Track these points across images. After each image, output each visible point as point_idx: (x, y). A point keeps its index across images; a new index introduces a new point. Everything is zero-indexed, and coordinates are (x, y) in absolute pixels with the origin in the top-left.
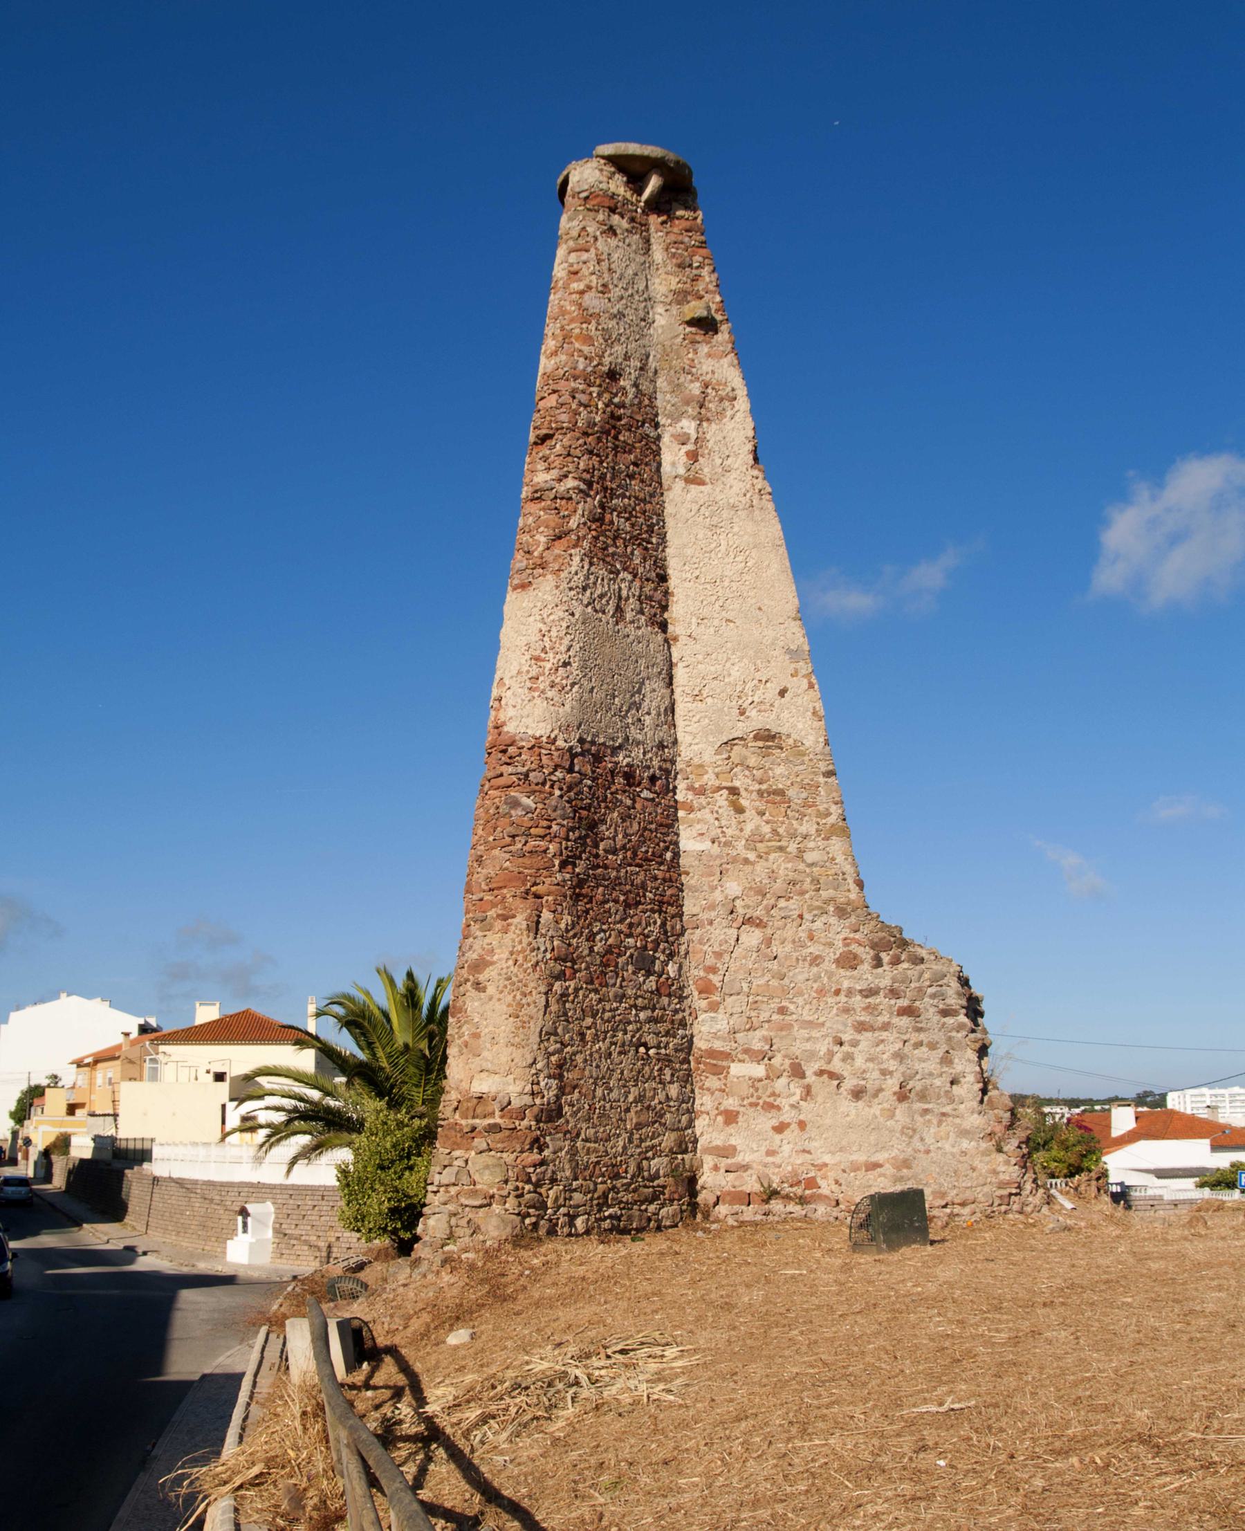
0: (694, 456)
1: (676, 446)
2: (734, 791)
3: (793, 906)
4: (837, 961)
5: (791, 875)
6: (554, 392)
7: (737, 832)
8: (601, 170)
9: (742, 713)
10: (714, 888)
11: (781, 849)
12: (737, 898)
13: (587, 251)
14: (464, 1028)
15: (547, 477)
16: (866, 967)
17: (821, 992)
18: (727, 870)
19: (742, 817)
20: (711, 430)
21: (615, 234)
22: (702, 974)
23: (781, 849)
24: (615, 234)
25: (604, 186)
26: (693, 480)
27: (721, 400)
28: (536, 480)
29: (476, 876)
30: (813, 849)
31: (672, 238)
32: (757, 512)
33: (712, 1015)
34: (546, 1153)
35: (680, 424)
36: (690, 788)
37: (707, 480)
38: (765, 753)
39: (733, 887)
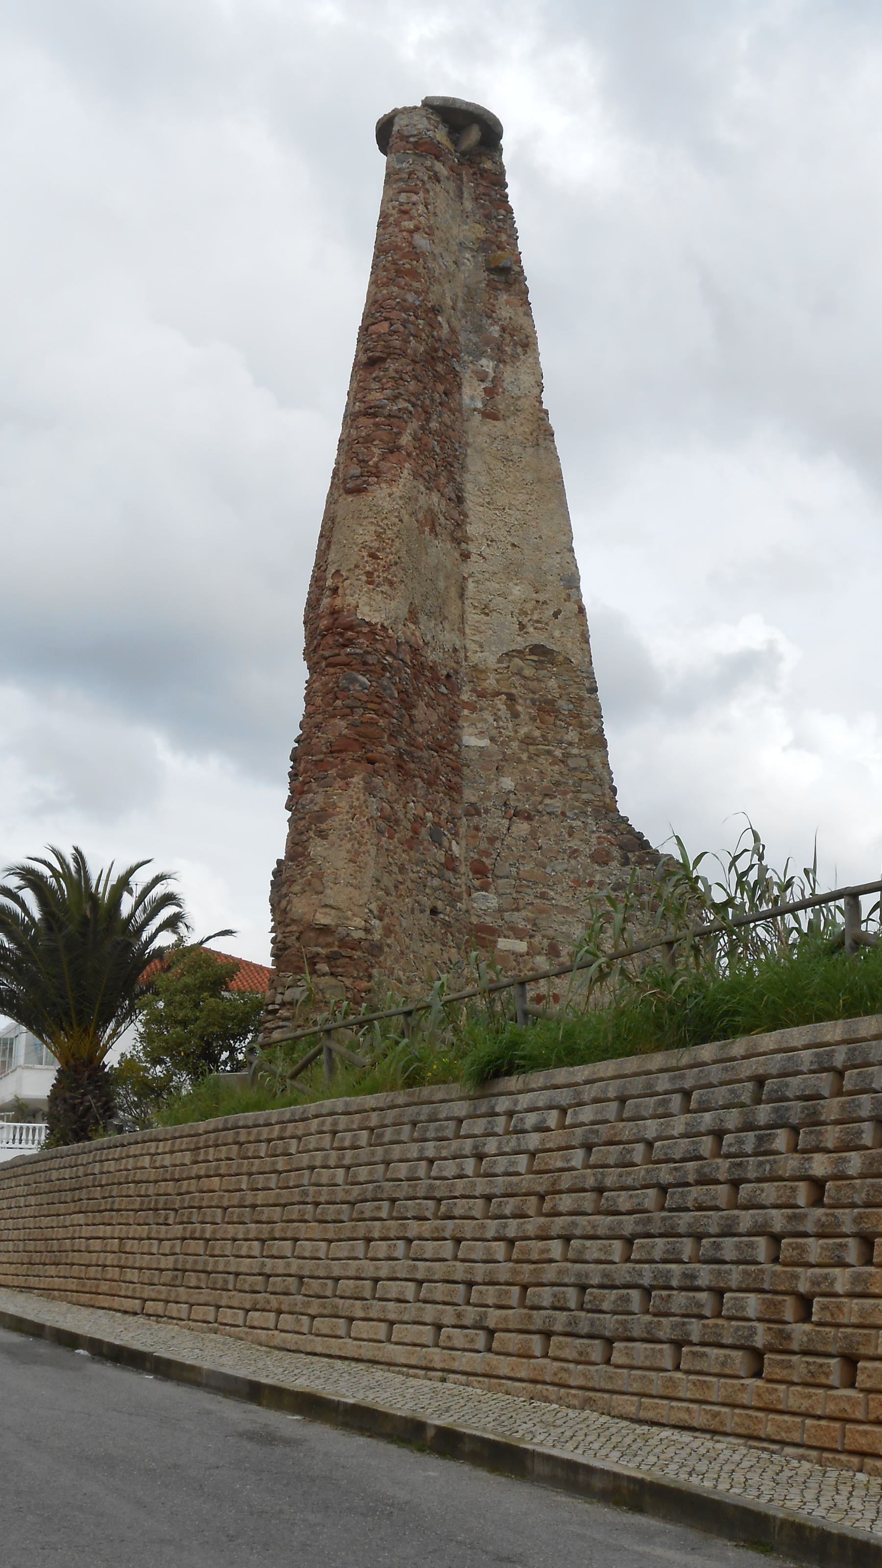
0: (490, 393)
1: (475, 382)
2: (511, 697)
3: (556, 804)
4: (591, 856)
5: (557, 777)
6: (386, 319)
7: (512, 734)
8: (428, 118)
9: (521, 629)
10: (490, 782)
11: (549, 752)
12: (510, 792)
13: (417, 193)
14: (307, 869)
15: (379, 395)
16: (614, 864)
17: (578, 882)
18: (503, 767)
19: (518, 721)
20: (508, 373)
21: (439, 181)
22: (476, 857)
23: (549, 752)
24: (439, 181)
25: (430, 133)
26: (490, 415)
27: (515, 345)
28: (370, 397)
29: (315, 740)
30: (576, 756)
31: (481, 190)
32: (542, 451)
33: (484, 893)
34: (372, 983)
35: (481, 362)
36: (474, 691)
37: (501, 417)
38: (539, 665)
39: (508, 783)
